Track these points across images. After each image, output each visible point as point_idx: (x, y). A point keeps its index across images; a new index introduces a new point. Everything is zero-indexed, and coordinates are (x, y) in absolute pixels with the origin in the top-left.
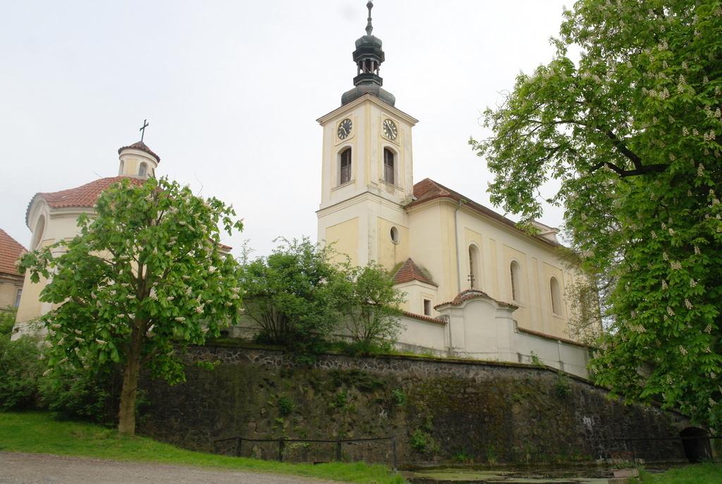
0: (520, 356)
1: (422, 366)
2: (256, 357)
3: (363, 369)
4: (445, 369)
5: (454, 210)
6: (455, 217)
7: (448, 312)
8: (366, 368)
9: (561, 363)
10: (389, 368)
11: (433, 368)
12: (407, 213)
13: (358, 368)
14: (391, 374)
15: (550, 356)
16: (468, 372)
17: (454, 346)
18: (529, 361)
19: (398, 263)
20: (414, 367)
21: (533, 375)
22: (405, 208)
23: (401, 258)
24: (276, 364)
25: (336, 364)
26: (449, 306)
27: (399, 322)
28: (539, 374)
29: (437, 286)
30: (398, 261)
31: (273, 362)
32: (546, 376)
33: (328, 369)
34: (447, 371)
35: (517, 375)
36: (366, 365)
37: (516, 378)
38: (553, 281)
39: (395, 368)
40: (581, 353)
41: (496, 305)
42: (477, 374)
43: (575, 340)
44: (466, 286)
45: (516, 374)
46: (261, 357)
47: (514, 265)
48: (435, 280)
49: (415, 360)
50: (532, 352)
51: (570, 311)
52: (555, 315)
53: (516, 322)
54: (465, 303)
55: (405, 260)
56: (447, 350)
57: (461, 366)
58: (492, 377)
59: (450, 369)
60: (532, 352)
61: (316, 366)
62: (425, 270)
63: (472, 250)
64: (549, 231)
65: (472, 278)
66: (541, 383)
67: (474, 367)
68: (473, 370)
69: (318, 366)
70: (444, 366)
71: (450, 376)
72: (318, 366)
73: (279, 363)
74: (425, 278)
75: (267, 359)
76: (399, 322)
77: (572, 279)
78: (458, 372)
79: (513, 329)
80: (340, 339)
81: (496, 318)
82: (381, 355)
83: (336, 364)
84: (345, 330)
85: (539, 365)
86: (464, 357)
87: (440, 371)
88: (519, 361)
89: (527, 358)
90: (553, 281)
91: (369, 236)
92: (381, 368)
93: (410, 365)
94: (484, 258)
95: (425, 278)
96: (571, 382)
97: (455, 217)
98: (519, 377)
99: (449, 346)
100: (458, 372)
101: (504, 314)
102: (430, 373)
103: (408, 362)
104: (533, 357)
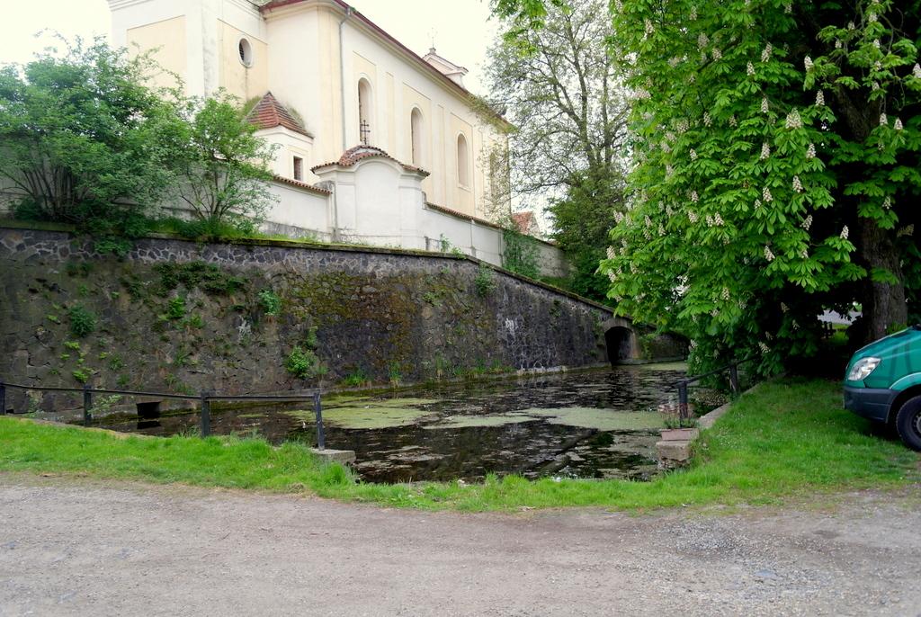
0: (428, 240)
1: (301, 257)
2: (18, 242)
3: (211, 261)
4: (334, 260)
5: (339, 22)
6: (340, 33)
7: (333, 177)
8: (215, 259)
9: (473, 248)
10: (252, 259)
11: (316, 258)
12: (265, 19)
13: (203, 260)
14: (255, 267)
15: (463, 240)
16: (365, 264)
17: (340, 226)
18: (438, 247)
19: (251, 98)
20: (289, 258)
21: (449, 268)
22: (261, 9)
23: (257, 91)
24: (58, 254)
25: (166, 254)
26: (335, 168)
27: (268, 190)
28: (456, 265)
29: (312, 138)
30: (252, 95)
31: (52, 251)
32: (465, 268)
33: (152, 261)
34: (336, 263)
35: (430, 268)
36: (216, 255)
37: (429, 272)
38: (461, 140)
39: (261, 259)
40: (495, 236)
41: (400, 169)
42: (377, 267)
43: (488, 220)
44: (353, 141)
45: (428, 266)
46: (29, 243)
47: (415, 114)
48: (308, 129)
49: (290, 247)
50: (441, 235)
51: (480, 180)
52: (461, 186)
53: (425, 194)
54: (358, 164)
55: (262, 94)
56: (331, 231)
57: (357, 256)
58: (397, 271)
59: (341, 260)
60: (441, 235)
61: (131, 258)
62: (294, 112)
63: (362, 85)
64: (455, 71)
65: (363, 126)
66: (458, 277)
67: (373, 257)
68: (372, 261)
69: (135, 256)
70: (332, 255)
71: (341, 271)
72: (135, 256)
73: (64, 252)
74: (296, 126)
75: (40, 246)
76: (268, 190)
77: (484, 138)
78: (352, 264)
79: (421, 205)
80: (169, 214)
81: (400, 187)
82: (238, 240)
83: (166, 254)
84: (179, 200)
85: (458, 254)
86: (354, 241)
87: (327, 264)
88: (427, 248)
89: (435, 244)
90: (461, 140)
91: (205, 50)
92: (240, 260)
93: (284, 255)
94: (377, 98)
95: (296, 126)
96: (495, 276)
97: (340, 33)
98: (432, 270)
99: (334, 226)
100: (352, 264)
101: (411, 182)
102: (312, 266)
103: (280, 251)
104: (443, 242)
